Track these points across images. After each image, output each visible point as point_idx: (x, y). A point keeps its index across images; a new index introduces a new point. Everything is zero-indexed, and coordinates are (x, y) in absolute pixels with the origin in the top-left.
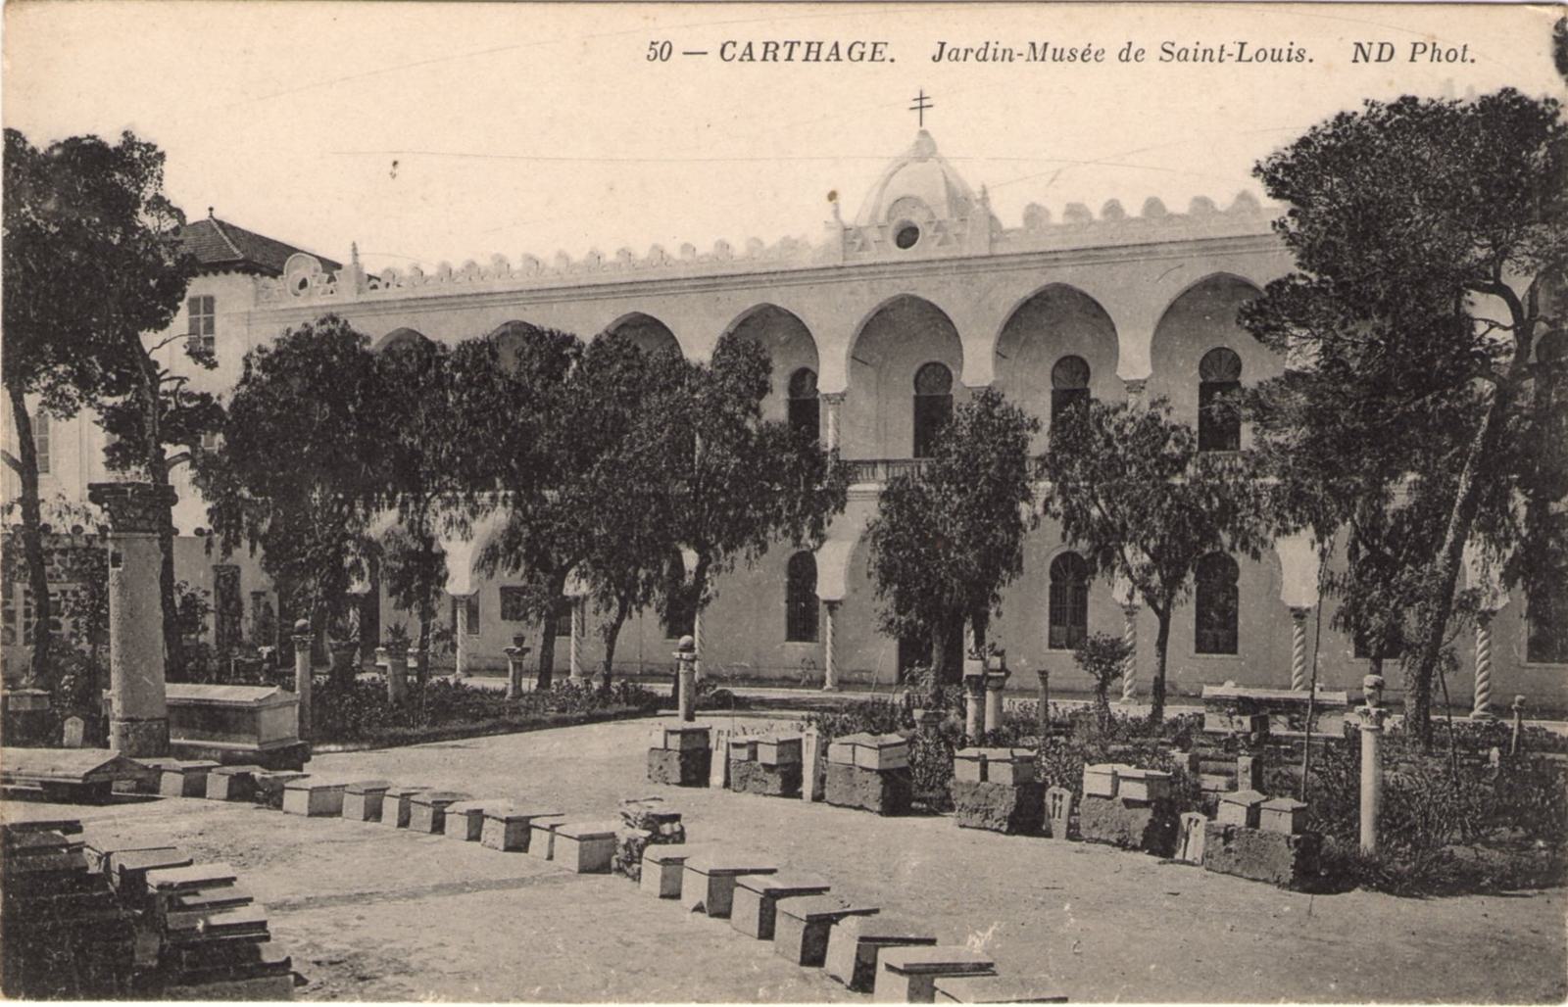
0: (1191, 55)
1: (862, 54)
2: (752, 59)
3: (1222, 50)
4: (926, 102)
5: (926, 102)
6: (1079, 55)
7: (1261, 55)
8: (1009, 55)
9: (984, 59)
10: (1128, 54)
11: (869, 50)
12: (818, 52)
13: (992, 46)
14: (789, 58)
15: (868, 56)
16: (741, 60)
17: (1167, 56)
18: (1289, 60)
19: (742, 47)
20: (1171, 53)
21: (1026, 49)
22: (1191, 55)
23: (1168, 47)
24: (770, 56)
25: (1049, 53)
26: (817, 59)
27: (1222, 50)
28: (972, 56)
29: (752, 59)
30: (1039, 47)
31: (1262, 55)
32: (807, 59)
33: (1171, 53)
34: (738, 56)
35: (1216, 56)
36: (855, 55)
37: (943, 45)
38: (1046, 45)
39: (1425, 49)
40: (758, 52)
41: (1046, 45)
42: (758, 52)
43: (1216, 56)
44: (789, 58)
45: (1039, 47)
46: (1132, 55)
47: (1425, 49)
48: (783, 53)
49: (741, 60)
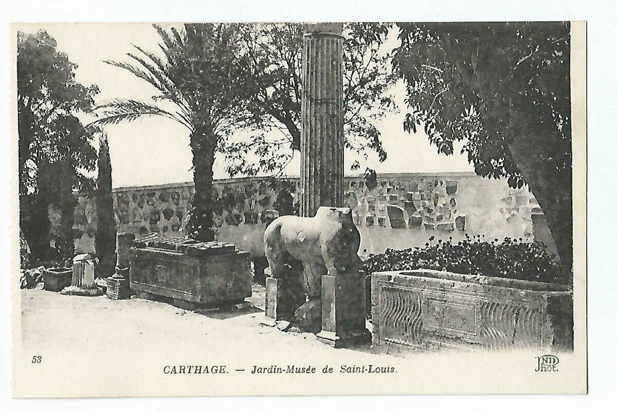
0: (352, 370)
1: (217, 370)
2: (175, 373)
3: (363, 368)
4: (243, 144)
5: (243, 144)
6: (306, 370)
7: (378, 370)
8: (280, 370)
9: (271, 372)
10: (327, 370)
11: (219, 369)
12: (200, 370)
13: (274, 367)
14: (189, 372)
15: (219, 371)
16: (171, 373)
17: (343, 371)
18: (275, 372)
19: (172, 368)
20: (344, 369)
21: (286, 368)
22: (352, 370)
23: (343, 367)
24: (182, 371)
25: (295, 370)
26: (200, 373)
27: (363, 368)
28: (266, 371)
29: (175, 373)
30: (291, 368)
31: (378, 370)
32: (196, 373)
33: (344, 369)
34: (170, 372)
35: (361, 370)
36: (214, 371)
37: (255, 367)
38: (293, 366)
39: (258, 370)
40: (178, 370)
41: (293, 366)
42: (178, 370)
43: (361, 370)
44: (189, 372)
45: (291, 368)
46: (328, 370)
47: (258, 370)
48: (187, 370)
49: (171, 373)
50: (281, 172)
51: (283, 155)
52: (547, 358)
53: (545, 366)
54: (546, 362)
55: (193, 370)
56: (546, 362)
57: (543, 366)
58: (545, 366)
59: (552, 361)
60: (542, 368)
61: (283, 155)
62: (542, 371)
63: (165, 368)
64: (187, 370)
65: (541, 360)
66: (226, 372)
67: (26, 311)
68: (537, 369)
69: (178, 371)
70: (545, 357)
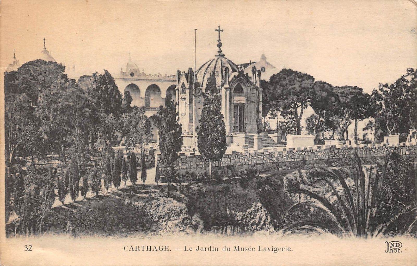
15: (164, 250)
31: (243, 250)
36: (161, 249)
42: (267, 249)
47: (288, 249)
50: (339, 191)
51: (162, 250)
52: (394, 243)
53: (392, 249)
54: (393, 246)
55: (145, 249)
56: (393, 246)
57: (391, 249)
58: (392, 249)
59: (398, 245)
60: (390, 250)
61: (162, 250)
62: (390, 252)
63: (159, 247)
64: (141, 249)
65: (390, 245)
66: (169, 250)
67: (277, 119)
68: (386, 251)
69: (134, 249)
70: (392, 243)
